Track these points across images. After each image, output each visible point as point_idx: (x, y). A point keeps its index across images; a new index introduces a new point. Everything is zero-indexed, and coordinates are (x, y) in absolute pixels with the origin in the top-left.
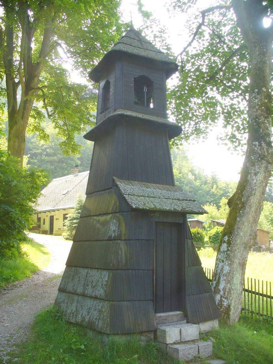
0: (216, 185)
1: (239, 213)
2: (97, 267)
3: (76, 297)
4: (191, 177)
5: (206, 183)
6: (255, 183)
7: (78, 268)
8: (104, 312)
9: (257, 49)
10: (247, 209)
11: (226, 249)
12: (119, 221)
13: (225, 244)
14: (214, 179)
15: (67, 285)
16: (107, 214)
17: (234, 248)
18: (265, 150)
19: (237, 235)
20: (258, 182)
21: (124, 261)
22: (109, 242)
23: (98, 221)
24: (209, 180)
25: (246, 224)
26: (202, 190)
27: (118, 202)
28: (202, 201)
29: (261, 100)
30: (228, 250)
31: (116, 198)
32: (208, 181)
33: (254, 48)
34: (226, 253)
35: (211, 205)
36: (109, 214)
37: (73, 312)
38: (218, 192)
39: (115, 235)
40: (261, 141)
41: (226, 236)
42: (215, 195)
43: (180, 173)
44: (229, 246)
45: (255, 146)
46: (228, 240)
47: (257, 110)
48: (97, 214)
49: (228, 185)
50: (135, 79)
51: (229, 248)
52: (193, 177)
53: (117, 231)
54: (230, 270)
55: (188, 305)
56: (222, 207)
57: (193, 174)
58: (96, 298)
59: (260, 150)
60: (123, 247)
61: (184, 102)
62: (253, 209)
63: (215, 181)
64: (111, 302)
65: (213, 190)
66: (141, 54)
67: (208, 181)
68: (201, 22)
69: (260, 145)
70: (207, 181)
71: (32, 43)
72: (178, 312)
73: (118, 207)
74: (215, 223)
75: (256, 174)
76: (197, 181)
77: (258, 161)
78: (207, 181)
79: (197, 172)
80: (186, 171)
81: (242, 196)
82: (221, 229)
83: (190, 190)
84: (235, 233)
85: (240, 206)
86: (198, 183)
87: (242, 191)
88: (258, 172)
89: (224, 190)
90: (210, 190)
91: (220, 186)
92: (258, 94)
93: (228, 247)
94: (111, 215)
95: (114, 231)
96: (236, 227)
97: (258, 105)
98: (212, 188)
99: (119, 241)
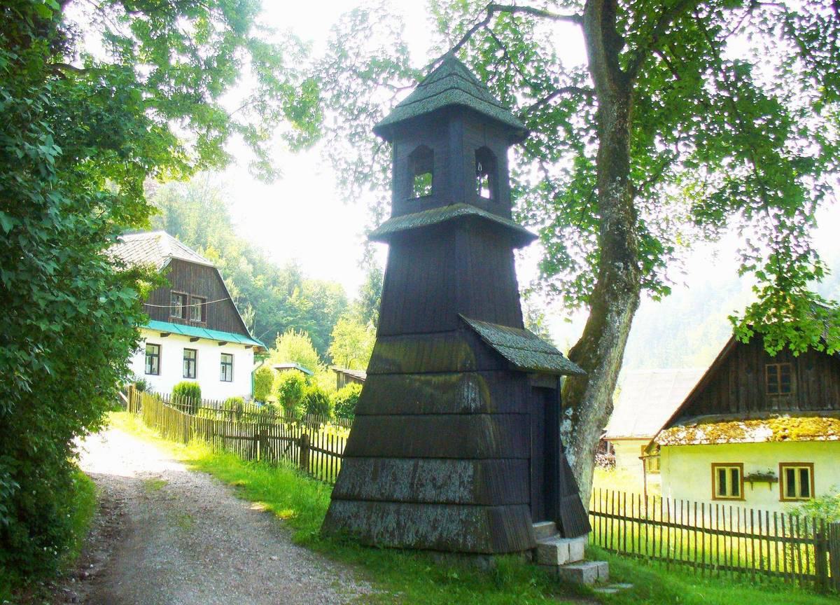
0: (299, 287)
1: (593, 372)
2: (441, 455)
3: (392, 507)
4: (245, 267)
5: (275, 283)
6: (618, 327)
7: (387, 461)
8: (477, 522)
9: (616, 107)
10: (606, 367)
11: (570, 429)
12: (478, 384)
13: (569, 422)
14: (293, 275)
15: (360, 488)
16: (449, 371)
17: (583, 428)
18: (633, 276)
19: (589, 407)
20: (623, 325)
21: (494, 446)
22: (463, 417)
23: (429, 383)
24: (284, 275)
25: (603, 390)
26: (268, 296)
27: (473, 355)
28: (267, 323)
29: (625, 194)
30: (574, 430)
31: (468, 349)
32: (281, 279)
33: (610, 105)
34: (569, 435)
35: (298, 333)
36: (456, 372)
37: (390, 529)
38: (302, 304)
39: (476, 405)
40: (627, 262)
41: (570, 409)
42: (295, 311)
43: (221, 257)
44: (576, 424)
45: (619, 268)
46: (574, 415)
47: (619, 210)
48: (423, 371)
49: (325, 289)
50: (476, 151)
51: (576, 428)
52: (251, 267)
53: (478, 399)
54: (577, 462)
55: (563, 512)
56: (337, 339)
57: (251, 261)
58: (449, 503)
59: (627, 276)
60: (488, 422)
61: (185, 69)
62: (613, 368)
63: (295, 281)
64: (487, 508)
65: (292, 300)
66: (472, 105)
67: (281, 279)
68: (482, 20)
69: (626, 268)
70: (278, 277)
71: (187, 17)
72: (551, 523)
73: (474, 362)
74: (341, 375)
75: (619, 314)
76: (259, 277)
77: (623, 292)
78: (278, 277)
79: (255, 257)
80: (235, 254)
81: (598, 346)
82: (358, 388)
83: (242, 295)
84: (585, 404)
85: (594, 361)
86: (259, 282)
87: (597, 339)
88: (622, 311)
89: (315, 299)
90: (284, 300)
91: (305, 292)
92: (621, 185)
93: (573, 426)
94: (460, 375)
95: (474, 400)
96: (587, 394)
97: (621, 202)
98: (290, 294)
99: (483, 416)
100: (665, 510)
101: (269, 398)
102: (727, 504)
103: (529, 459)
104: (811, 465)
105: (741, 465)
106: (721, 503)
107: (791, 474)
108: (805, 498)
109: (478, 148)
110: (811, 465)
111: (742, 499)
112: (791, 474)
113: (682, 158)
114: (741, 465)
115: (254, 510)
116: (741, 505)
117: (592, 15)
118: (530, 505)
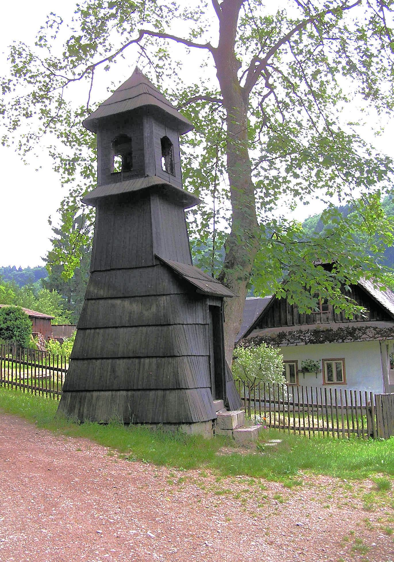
72: (220, 401)
100: (305, 395)
101: (115, 12)
102: (333, 387)
103: (209, 356)
104: (343, 360)
105: (296, 362)
106: (328, 387)
107: (329, 367)
108: (340, 382)
109: (162, 138)
110: (343, 360)
111: (345, 383)
112: (329, 367)
113: (322, 75)
114: (296, 362)
115: (280, 439)
116: (342, 387)
117: (174, 130)
118: (211, 388)
